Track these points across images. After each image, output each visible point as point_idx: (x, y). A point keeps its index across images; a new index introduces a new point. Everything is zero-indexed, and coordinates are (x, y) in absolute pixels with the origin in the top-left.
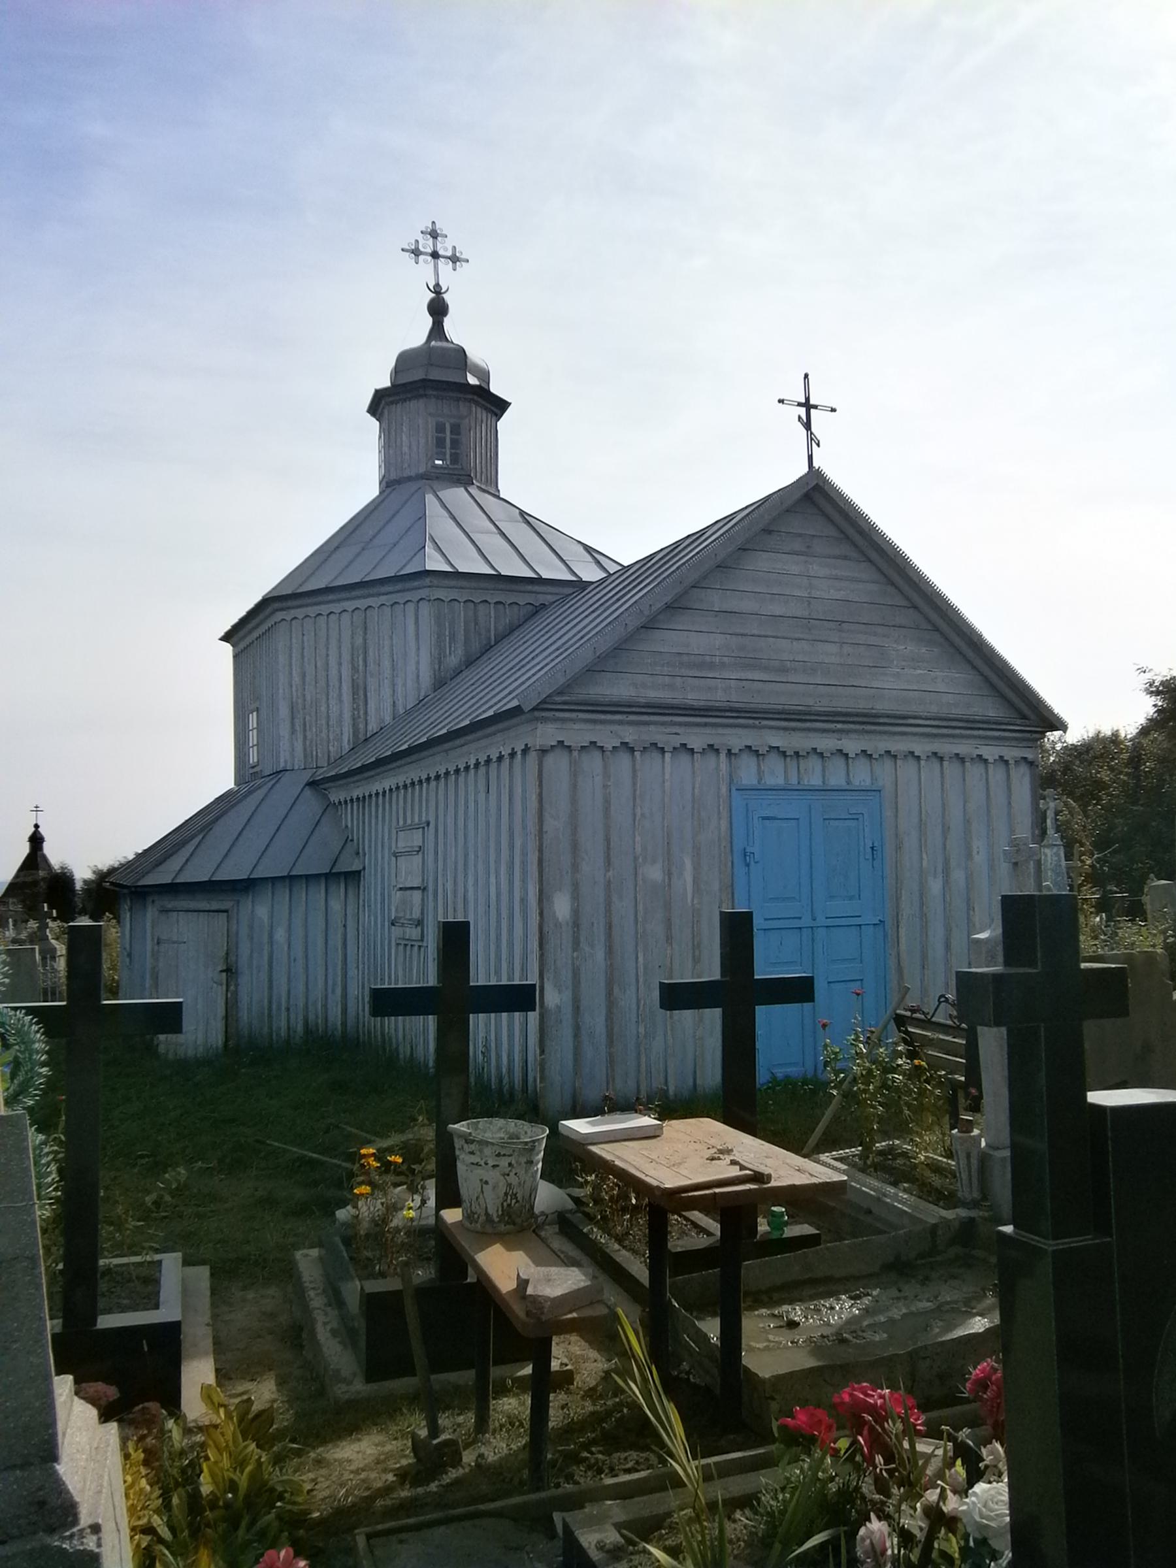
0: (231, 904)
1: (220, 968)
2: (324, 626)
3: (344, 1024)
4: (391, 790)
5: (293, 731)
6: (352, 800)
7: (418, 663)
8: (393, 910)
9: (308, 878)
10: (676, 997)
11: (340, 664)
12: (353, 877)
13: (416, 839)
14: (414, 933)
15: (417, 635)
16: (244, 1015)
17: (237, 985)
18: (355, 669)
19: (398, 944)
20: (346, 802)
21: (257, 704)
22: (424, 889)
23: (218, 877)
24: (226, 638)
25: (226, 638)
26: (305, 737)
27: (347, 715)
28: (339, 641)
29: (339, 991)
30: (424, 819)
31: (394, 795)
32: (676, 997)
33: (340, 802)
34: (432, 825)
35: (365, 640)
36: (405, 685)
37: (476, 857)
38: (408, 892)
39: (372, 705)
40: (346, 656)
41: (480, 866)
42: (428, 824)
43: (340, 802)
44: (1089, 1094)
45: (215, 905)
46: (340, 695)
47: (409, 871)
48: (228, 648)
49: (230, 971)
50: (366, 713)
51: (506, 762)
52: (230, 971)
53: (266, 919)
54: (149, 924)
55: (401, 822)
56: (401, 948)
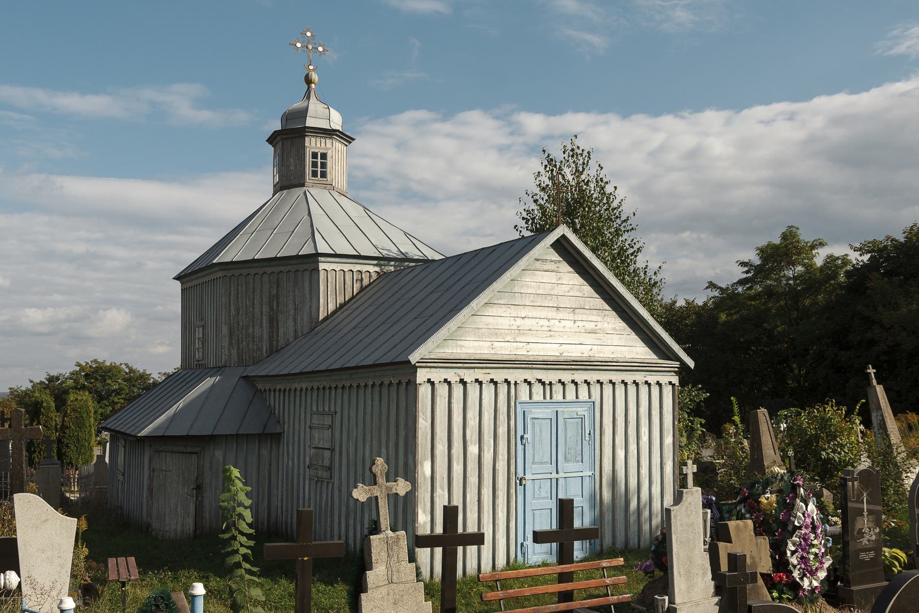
0: (199, 449)
1: (192, 487)
2: (251, 281)
3: (269, 521)
4: (307, 389)
5: (231, 343)
6: (275, 390)
7: (310, 307)
8: (307, 460)
9: (248, 436)
10: (539, 537)
11: (262, 305)
12: (276, 438)
13: (327, 421)
14: (325, 474)
15: (310, 290)
16: (207, 515)
17: (202, 497)
18: (271, 308)
19: (310, 479)
20: (270, 390)
21: (203, 323)
22: (332, 450)
23: (194, 432)
24: (178, 278)
25: (178, 278)
26: (239, 348)
27: (265, 336)
28: (261, 291)
29: (266, 502)
30: (332, 409)
31: (309, 394)
32: (539, 537)
33: (265, 390)
34: (339, 415)
35: (277, 291)
36: (302, 320)
37: (372, 436)
38: (321, 451)
39: (281, 331)
40: (265, 300)
41: (375, 442)
42: (336, 413)
43: (265, 390)
44: (441, 549)
45: (189, 450)
46: (261, 323)
47: (322, 438)
48: (178, 284)
49: (199, 488)
50: (278, 335)
51: (394, 389)
52: (199, 488)
53: (221, 459)
54: (146, 459)
55: (314, 409)
56: (313, 483)
